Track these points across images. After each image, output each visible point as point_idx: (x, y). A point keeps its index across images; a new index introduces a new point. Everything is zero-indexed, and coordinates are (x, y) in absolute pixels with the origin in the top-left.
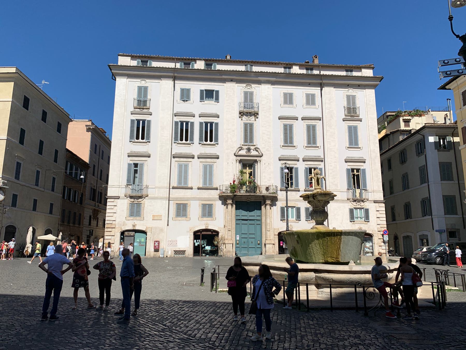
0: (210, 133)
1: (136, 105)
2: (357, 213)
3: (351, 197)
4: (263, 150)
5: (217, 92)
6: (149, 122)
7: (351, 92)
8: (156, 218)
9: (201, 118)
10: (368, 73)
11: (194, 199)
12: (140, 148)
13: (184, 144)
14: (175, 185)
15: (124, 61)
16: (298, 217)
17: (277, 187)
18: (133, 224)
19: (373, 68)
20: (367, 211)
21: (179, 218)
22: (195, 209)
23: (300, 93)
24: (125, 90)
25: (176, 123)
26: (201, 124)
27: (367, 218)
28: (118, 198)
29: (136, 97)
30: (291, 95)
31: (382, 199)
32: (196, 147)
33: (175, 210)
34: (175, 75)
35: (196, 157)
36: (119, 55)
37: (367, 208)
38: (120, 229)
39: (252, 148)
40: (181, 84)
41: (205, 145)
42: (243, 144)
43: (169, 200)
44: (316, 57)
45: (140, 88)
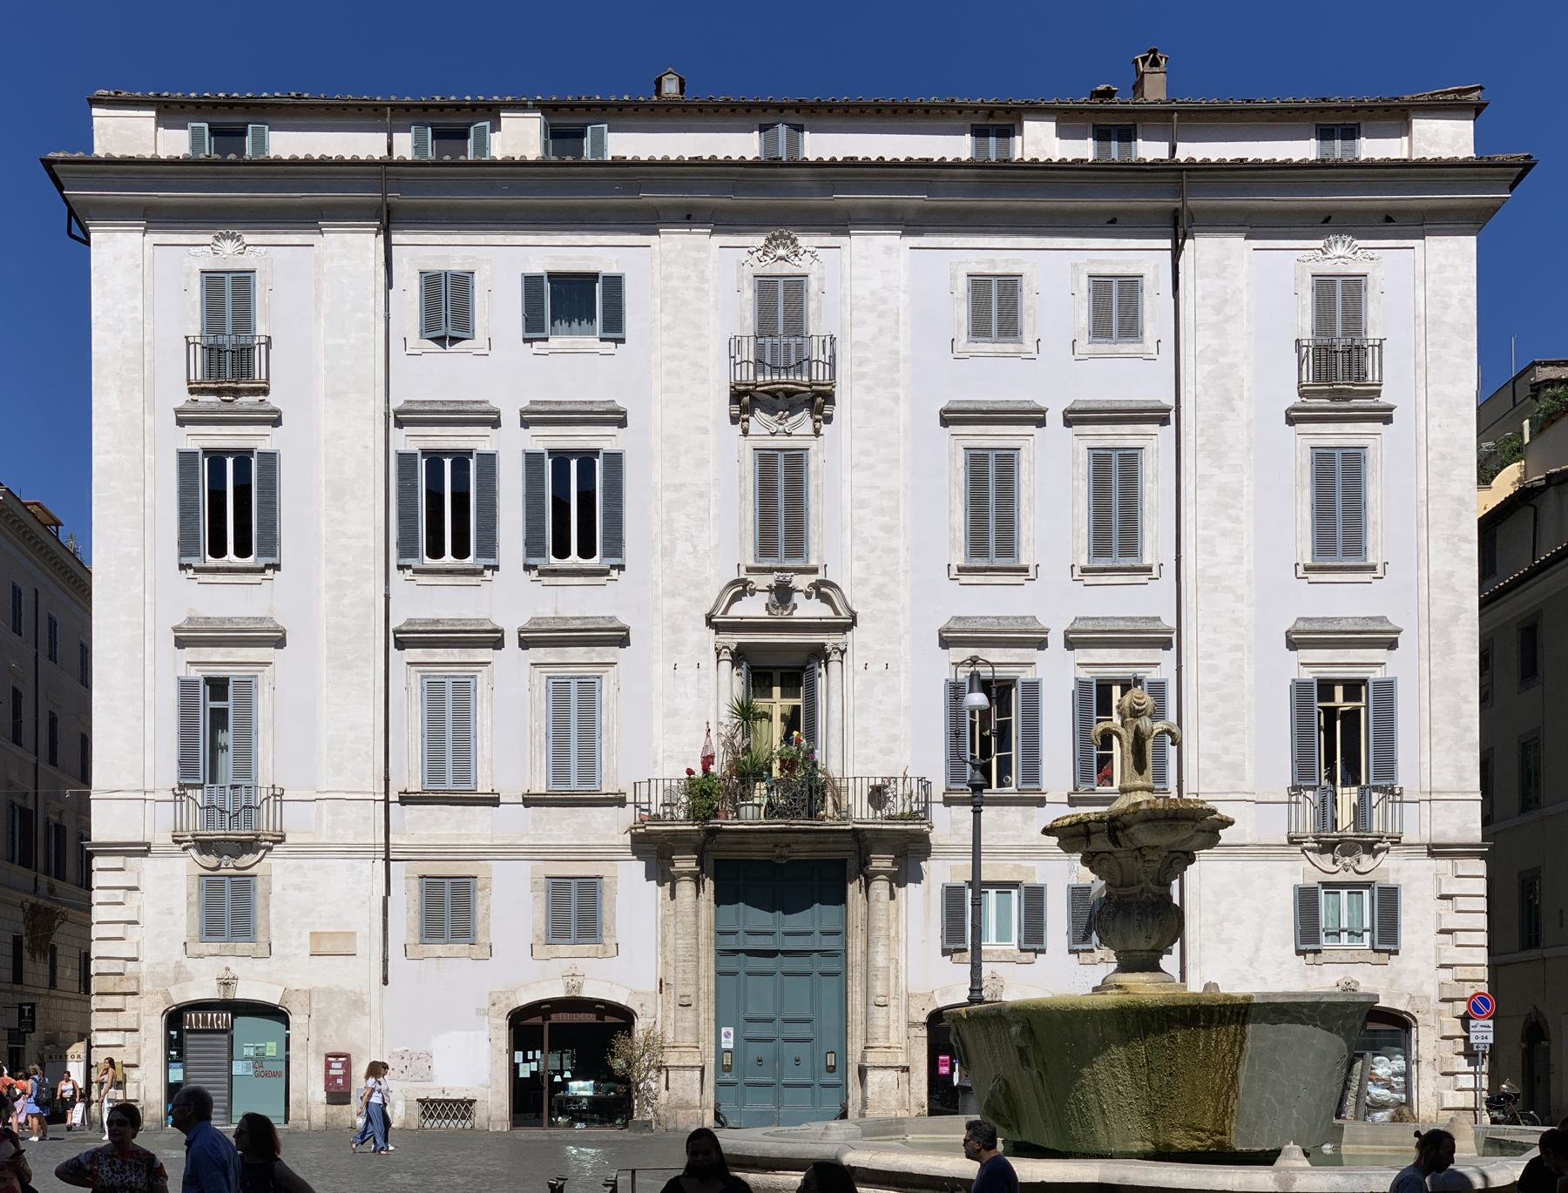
0: (579, 510)
1: (198, 373)
4: (855, 595)
5: (615, 284)
6: (270, 460)
11: (509, 853)
12: (229, 598)
14: (415, 786)
16: (1033, 937)
18: (222, 973)
20: (1388, 900)
24: (141, 287)
25: (406, 461)
26: (532, 461)
27: (1387, 933)
29: (195, 328)
30: (1010, 285)
32: (510, 593)
34: (385, 201)
37: (1392, 882)
38: (159, 997)
39: (801, 582)
40: (423, 252)
41: (555, 572)
45: (213, 280)
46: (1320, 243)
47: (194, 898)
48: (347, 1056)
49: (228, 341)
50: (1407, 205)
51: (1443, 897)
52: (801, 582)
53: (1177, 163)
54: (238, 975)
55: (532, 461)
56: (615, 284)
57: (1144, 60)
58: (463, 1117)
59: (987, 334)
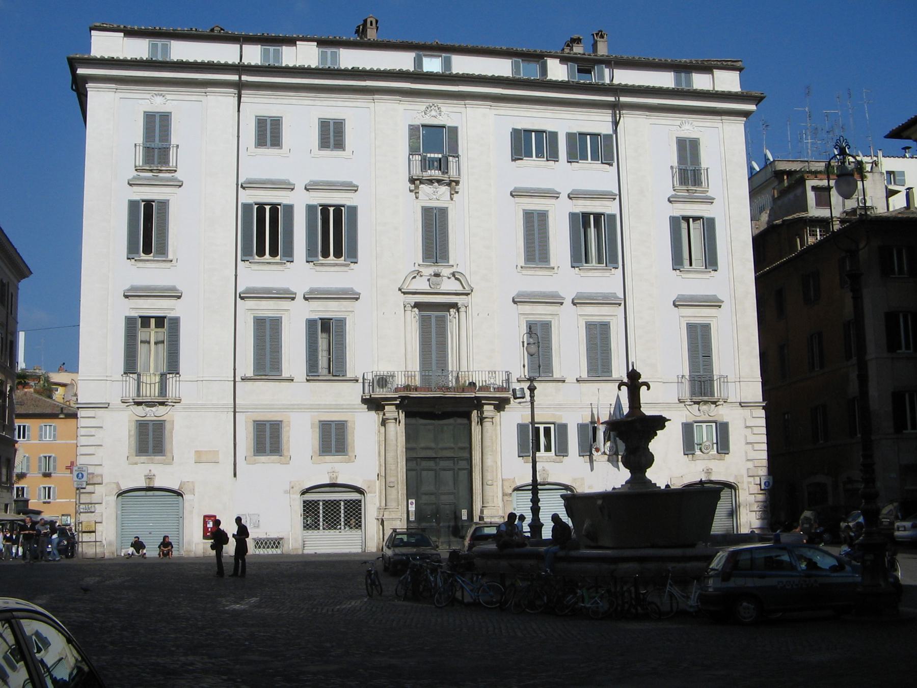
0: (335, 232)
1: (140, 162)
2: (705, 435)
3: (133, 393)
4: (473, 280)
5: (454, 131)
6: (353, 210)
7: (691, 127)
8: (200, 458)
9: (135, 188)
10: (728, 81)
11: (299, 408)
12: (149, 273)
13: (269, 263)
14: (250, 373)
15: (105, 44)
16: (563, 450)
17: (508, 374)
18: (147, 472)
19: (740, 69)
20: (723, 429)
21: (263, 458)
22: (301, 437)
23: (301, 115)
24: (113, 120)
25: (247, 207)
26: (311, 209)
27: (723, 445)
28: (106, 406)
29: (140, 140)
30: (276, 123)
31: (759, 397)
32: (299, 273)
33: (251, 436)
34: (240, 80)
35: (299, 297)
36: (91, 29)
37: (564, 422)
38: (115, 486)
39: (446, 272)
40: (259, 104)
41: (322, 265)
42: (523, 265)
43: (235, 412)
44: (602, 37)
45: (150, 117)
46: (678, 123)
47: (133, 432)
48: (205, 517)
49: (157, 143)
50: (713, 104)
51: (747, 427)
52: (446, 272)
53: (613, 85)
54: (156, 473)
55: (311, 209)
56: (454, 131)
57: (597, 34)
58: (277, 547)
59: (328, 147)
